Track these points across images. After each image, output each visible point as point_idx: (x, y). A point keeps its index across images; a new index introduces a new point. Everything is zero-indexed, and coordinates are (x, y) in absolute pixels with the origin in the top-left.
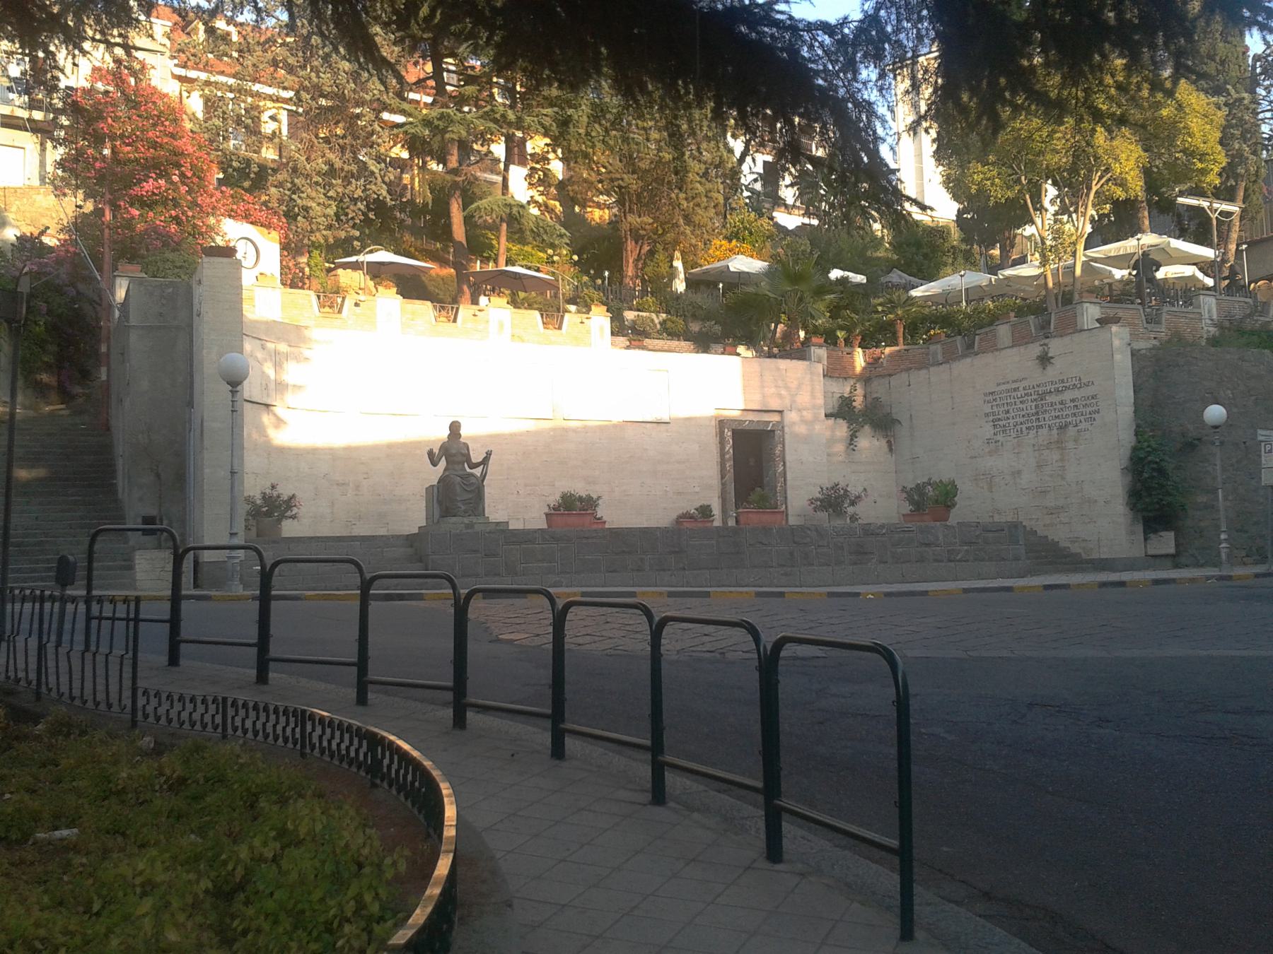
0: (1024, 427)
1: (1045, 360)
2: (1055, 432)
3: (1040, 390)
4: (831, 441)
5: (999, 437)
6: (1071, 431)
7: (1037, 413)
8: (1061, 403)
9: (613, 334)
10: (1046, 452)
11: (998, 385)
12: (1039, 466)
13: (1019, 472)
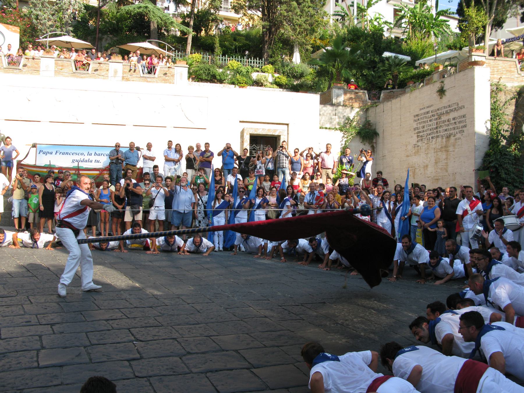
0: (430, 136)
1: (442, 92)
2: (444, 140)
3: (439, 112)
4: (512, 259)
5: (419, 144)
6: (452, 139)
7: (437, 128)
8: (448, 121)
9: (321, 103)
10: (440, 153)
11: (421, 109)
12: (436, 163)
13: (427, 166)
